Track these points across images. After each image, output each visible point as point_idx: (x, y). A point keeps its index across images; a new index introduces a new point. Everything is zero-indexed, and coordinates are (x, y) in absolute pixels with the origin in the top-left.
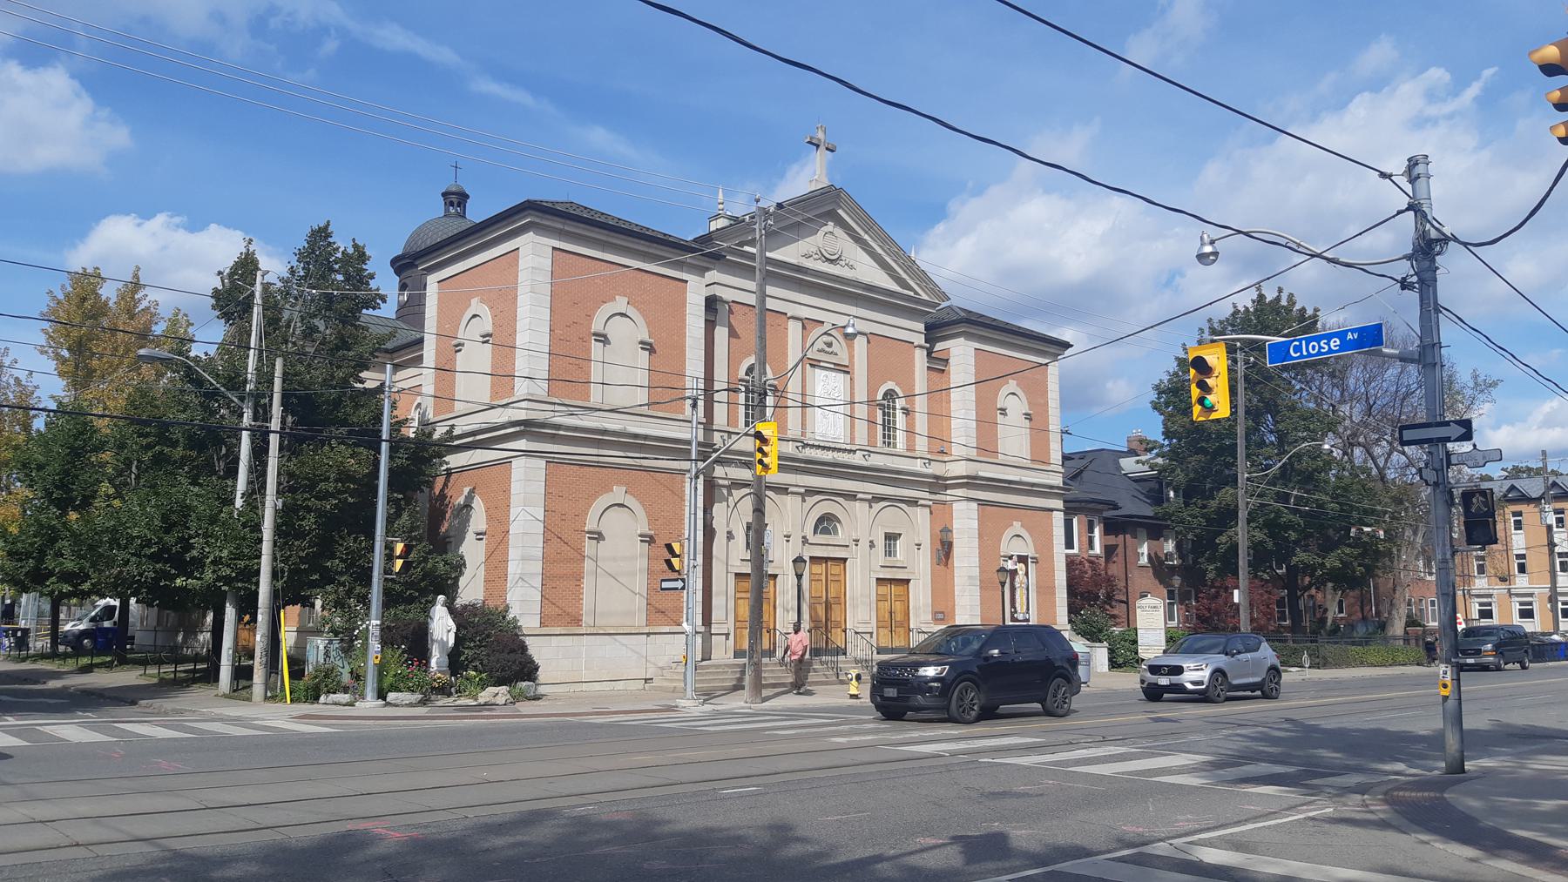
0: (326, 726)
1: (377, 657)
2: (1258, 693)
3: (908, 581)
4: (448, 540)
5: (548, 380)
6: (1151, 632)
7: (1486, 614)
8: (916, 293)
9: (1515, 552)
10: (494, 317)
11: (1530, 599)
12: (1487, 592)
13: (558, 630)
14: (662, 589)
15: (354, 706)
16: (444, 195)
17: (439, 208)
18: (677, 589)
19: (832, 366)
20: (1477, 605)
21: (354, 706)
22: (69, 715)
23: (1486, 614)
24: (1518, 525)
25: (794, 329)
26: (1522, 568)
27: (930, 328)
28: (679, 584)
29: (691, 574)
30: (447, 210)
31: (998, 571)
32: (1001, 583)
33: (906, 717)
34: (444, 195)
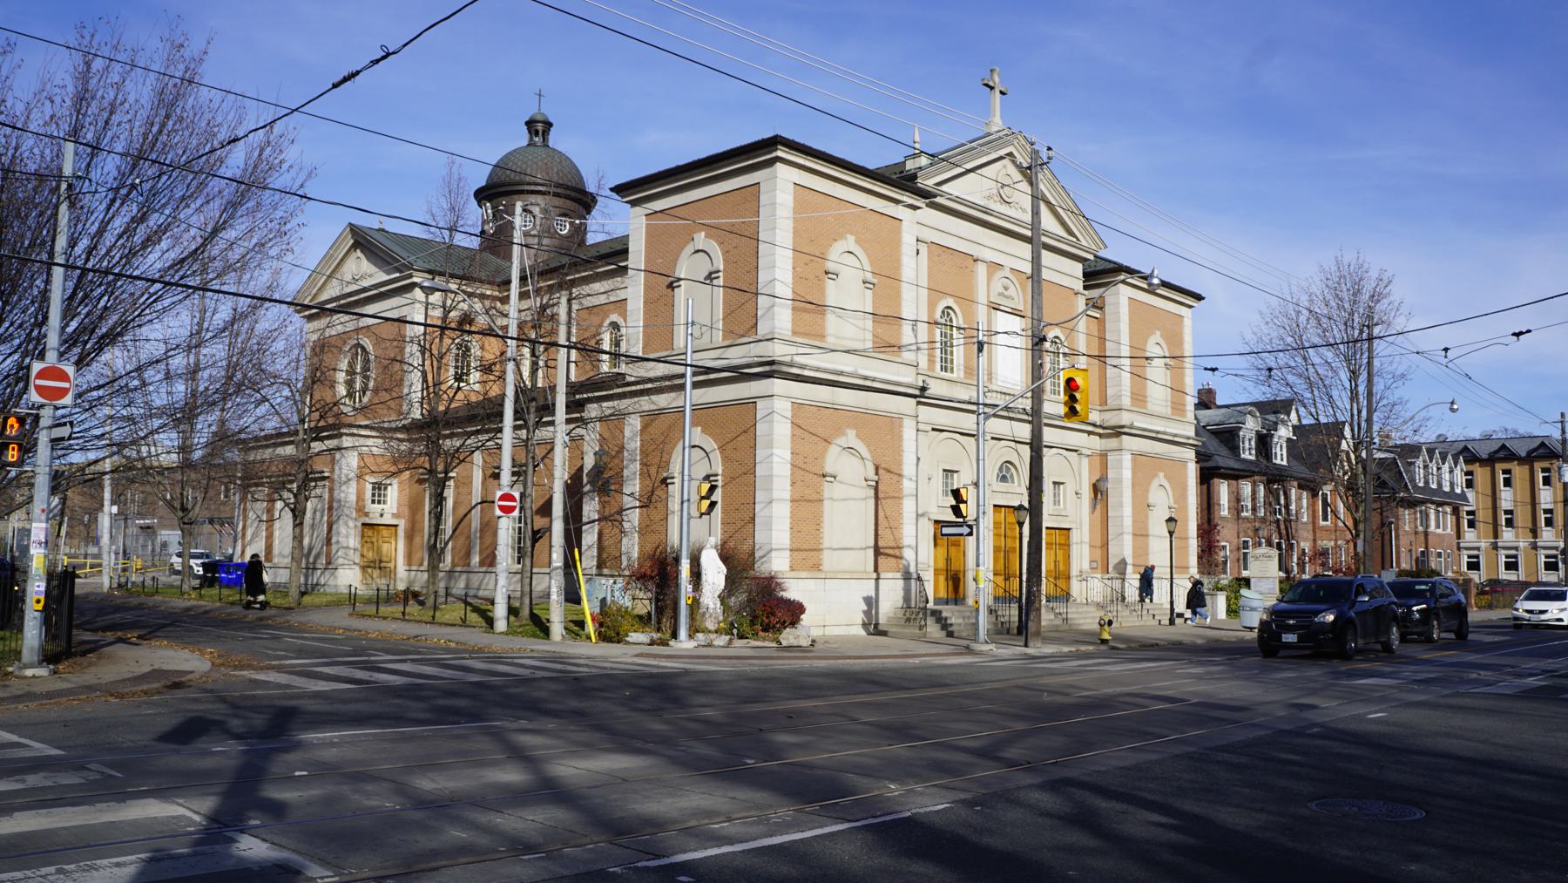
0: (717, 665)
1: (38, 601)
2: (1423, 638)
3: (1069, 529)
4: (669, 481)
5: (425, 325)
6: (1264, 580)
7: (1473, 566)
8: (1078, 240)
9: (1544, 506)
10: (725, 253)
11: (1475, 552)
12: (1514, 544)
13: (803, 574)
14: (942, 535)
15: (668, 645)
16: (527, 123)
17: (523, 139)
18: (962, 535)
19: (1010, 310)
20: (1543, 557)
21: (668, 645)
22: (1217, 641)
23: (1473, 566)
24: (1507, 483)
25: (981, 269)
26: (1509, 523)
27: (1088, 276)
28: (965, 530)
29: (981, 520)
30: (531, 139)
31: (1167, 521)
32: (1170, 532)
33: (1279, 655)
34: (527, 123)
